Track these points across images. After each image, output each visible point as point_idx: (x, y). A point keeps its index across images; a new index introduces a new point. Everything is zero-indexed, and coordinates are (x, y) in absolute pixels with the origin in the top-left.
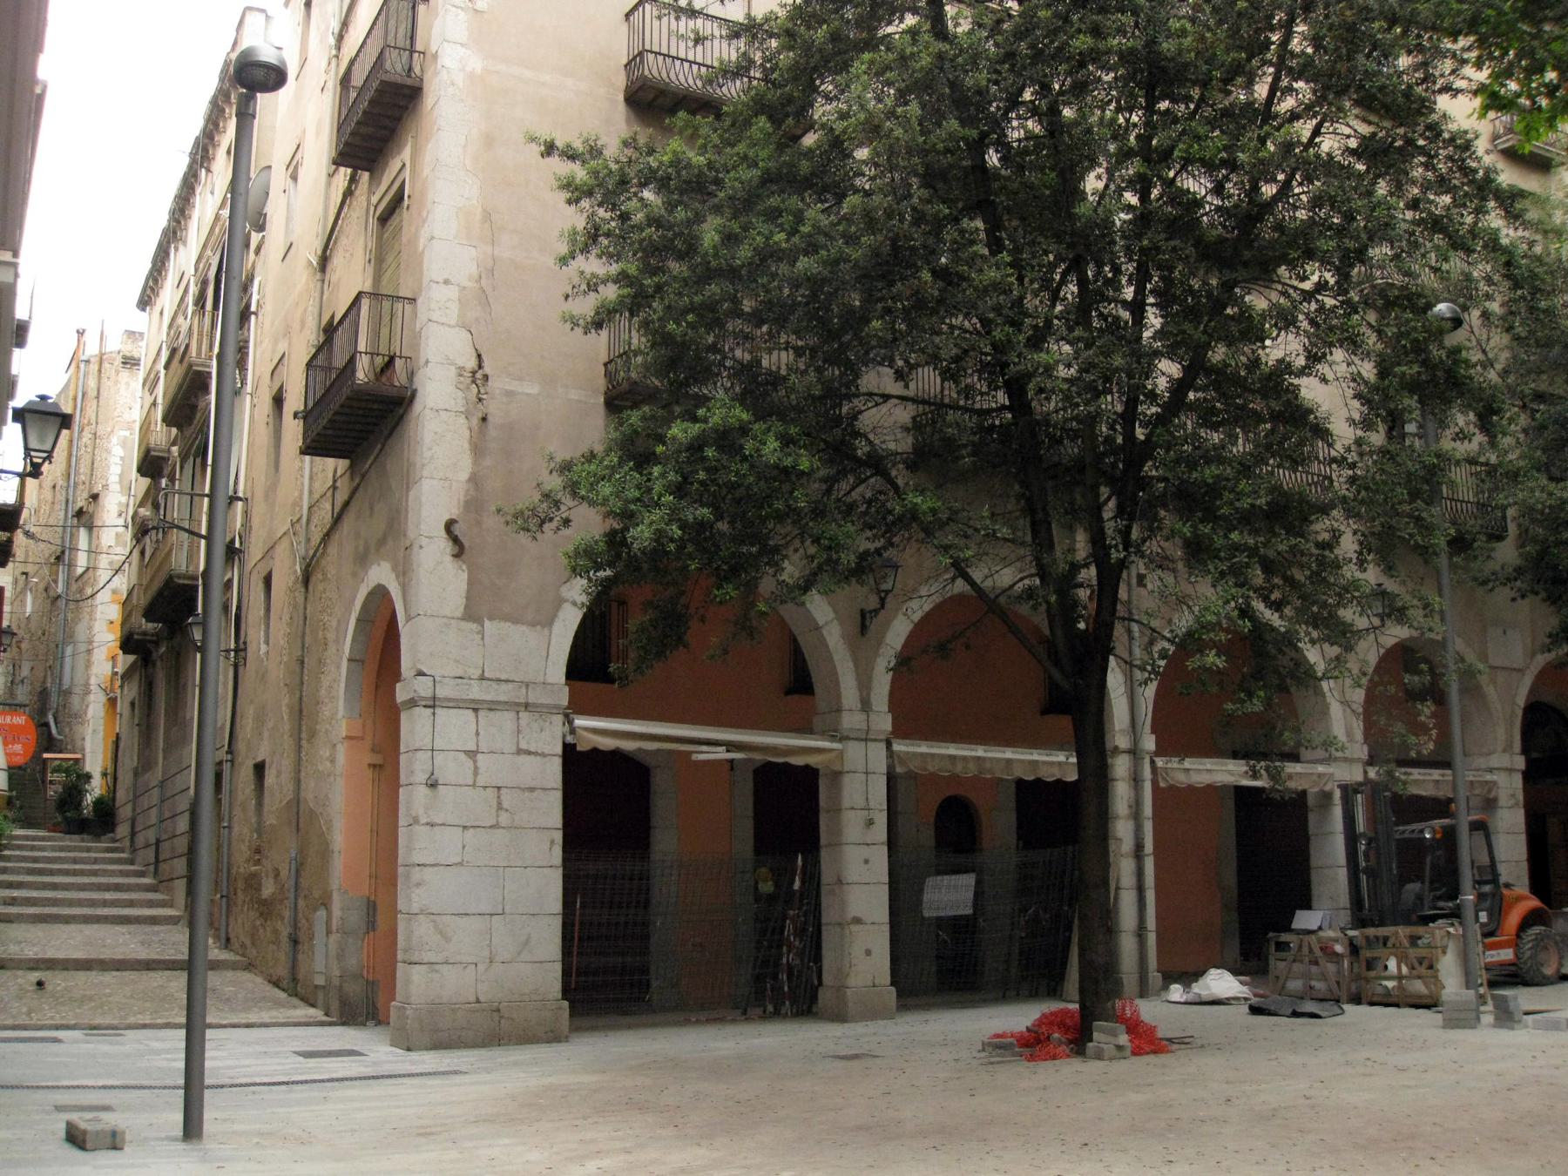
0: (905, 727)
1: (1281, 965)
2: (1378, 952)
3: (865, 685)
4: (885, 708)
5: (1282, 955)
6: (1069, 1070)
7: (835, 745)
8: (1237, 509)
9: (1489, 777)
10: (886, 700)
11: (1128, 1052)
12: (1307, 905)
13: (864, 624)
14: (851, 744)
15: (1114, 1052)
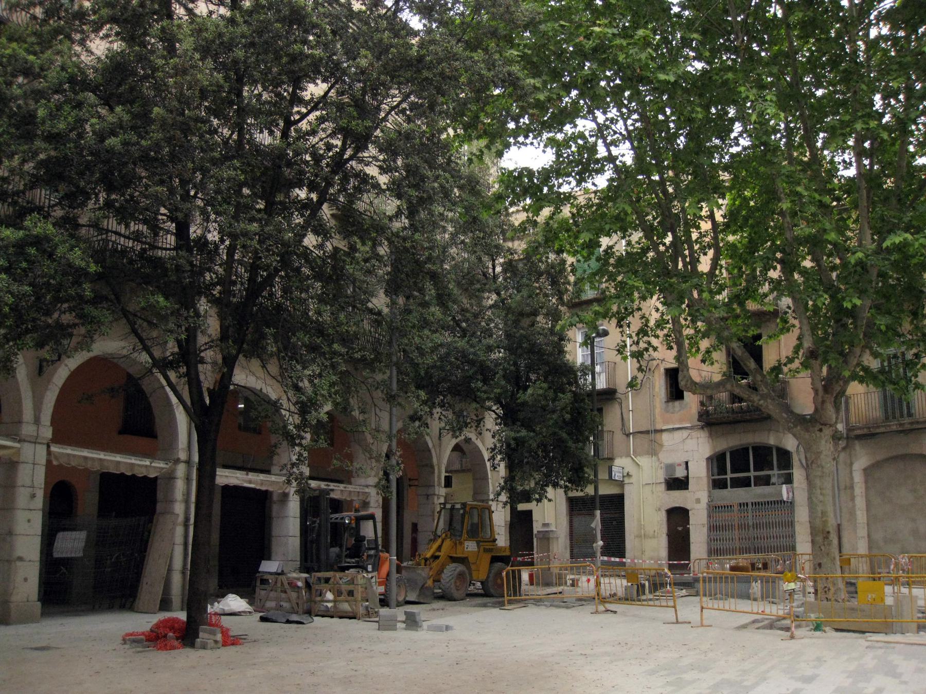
0: (59, 437)
1: (263, 592)
2: (323, 586)
3: (37, 408)
4: (48, 423)
5: (263, 586)
6: (185, 657)
7: (17, 445)
8: (337, 331)
9: (367, 490)
10: (49, 418)
11: (220, 645)
12: (269, 558)
13: (41, 369)
14: (26, 445)
15: (213, 644)
